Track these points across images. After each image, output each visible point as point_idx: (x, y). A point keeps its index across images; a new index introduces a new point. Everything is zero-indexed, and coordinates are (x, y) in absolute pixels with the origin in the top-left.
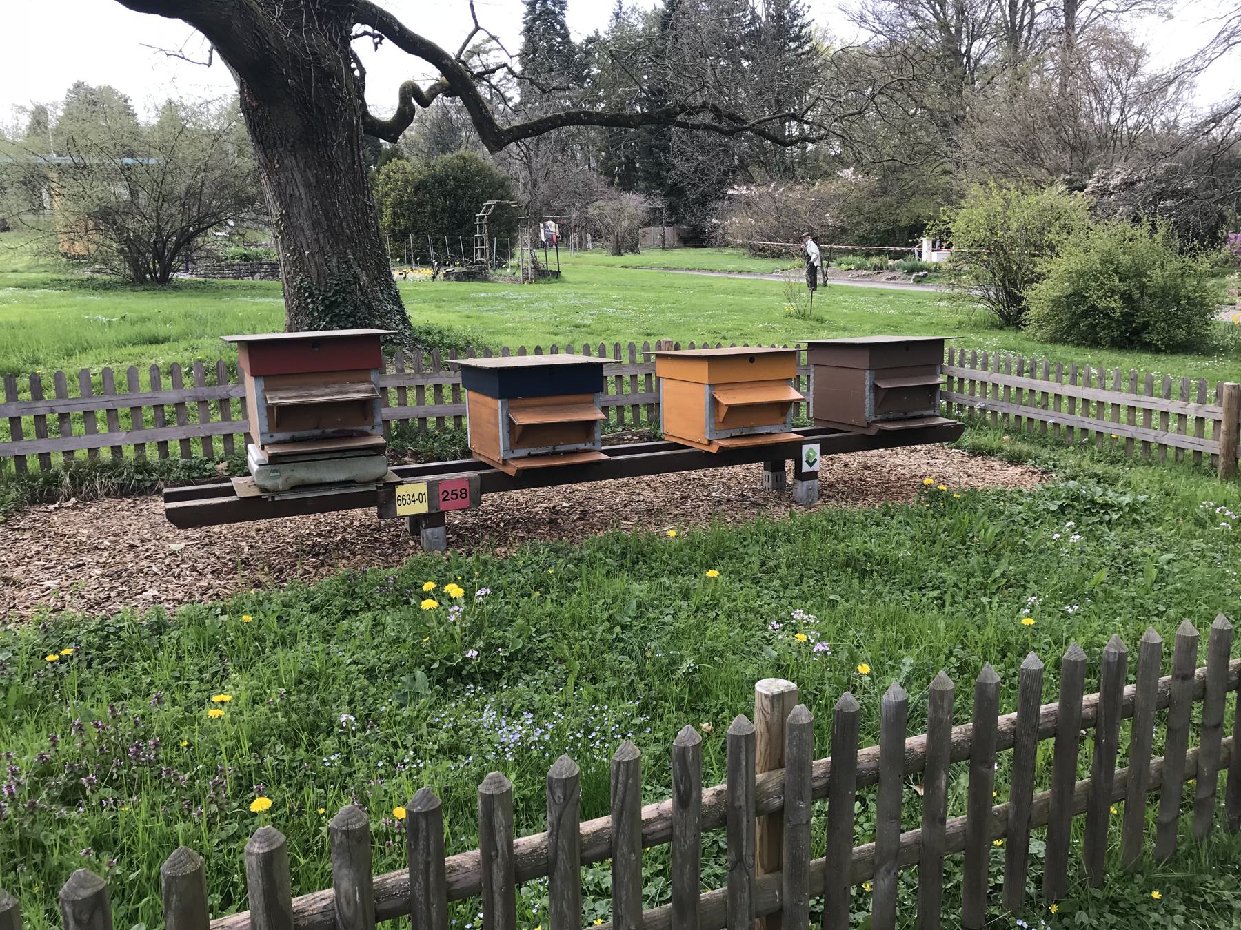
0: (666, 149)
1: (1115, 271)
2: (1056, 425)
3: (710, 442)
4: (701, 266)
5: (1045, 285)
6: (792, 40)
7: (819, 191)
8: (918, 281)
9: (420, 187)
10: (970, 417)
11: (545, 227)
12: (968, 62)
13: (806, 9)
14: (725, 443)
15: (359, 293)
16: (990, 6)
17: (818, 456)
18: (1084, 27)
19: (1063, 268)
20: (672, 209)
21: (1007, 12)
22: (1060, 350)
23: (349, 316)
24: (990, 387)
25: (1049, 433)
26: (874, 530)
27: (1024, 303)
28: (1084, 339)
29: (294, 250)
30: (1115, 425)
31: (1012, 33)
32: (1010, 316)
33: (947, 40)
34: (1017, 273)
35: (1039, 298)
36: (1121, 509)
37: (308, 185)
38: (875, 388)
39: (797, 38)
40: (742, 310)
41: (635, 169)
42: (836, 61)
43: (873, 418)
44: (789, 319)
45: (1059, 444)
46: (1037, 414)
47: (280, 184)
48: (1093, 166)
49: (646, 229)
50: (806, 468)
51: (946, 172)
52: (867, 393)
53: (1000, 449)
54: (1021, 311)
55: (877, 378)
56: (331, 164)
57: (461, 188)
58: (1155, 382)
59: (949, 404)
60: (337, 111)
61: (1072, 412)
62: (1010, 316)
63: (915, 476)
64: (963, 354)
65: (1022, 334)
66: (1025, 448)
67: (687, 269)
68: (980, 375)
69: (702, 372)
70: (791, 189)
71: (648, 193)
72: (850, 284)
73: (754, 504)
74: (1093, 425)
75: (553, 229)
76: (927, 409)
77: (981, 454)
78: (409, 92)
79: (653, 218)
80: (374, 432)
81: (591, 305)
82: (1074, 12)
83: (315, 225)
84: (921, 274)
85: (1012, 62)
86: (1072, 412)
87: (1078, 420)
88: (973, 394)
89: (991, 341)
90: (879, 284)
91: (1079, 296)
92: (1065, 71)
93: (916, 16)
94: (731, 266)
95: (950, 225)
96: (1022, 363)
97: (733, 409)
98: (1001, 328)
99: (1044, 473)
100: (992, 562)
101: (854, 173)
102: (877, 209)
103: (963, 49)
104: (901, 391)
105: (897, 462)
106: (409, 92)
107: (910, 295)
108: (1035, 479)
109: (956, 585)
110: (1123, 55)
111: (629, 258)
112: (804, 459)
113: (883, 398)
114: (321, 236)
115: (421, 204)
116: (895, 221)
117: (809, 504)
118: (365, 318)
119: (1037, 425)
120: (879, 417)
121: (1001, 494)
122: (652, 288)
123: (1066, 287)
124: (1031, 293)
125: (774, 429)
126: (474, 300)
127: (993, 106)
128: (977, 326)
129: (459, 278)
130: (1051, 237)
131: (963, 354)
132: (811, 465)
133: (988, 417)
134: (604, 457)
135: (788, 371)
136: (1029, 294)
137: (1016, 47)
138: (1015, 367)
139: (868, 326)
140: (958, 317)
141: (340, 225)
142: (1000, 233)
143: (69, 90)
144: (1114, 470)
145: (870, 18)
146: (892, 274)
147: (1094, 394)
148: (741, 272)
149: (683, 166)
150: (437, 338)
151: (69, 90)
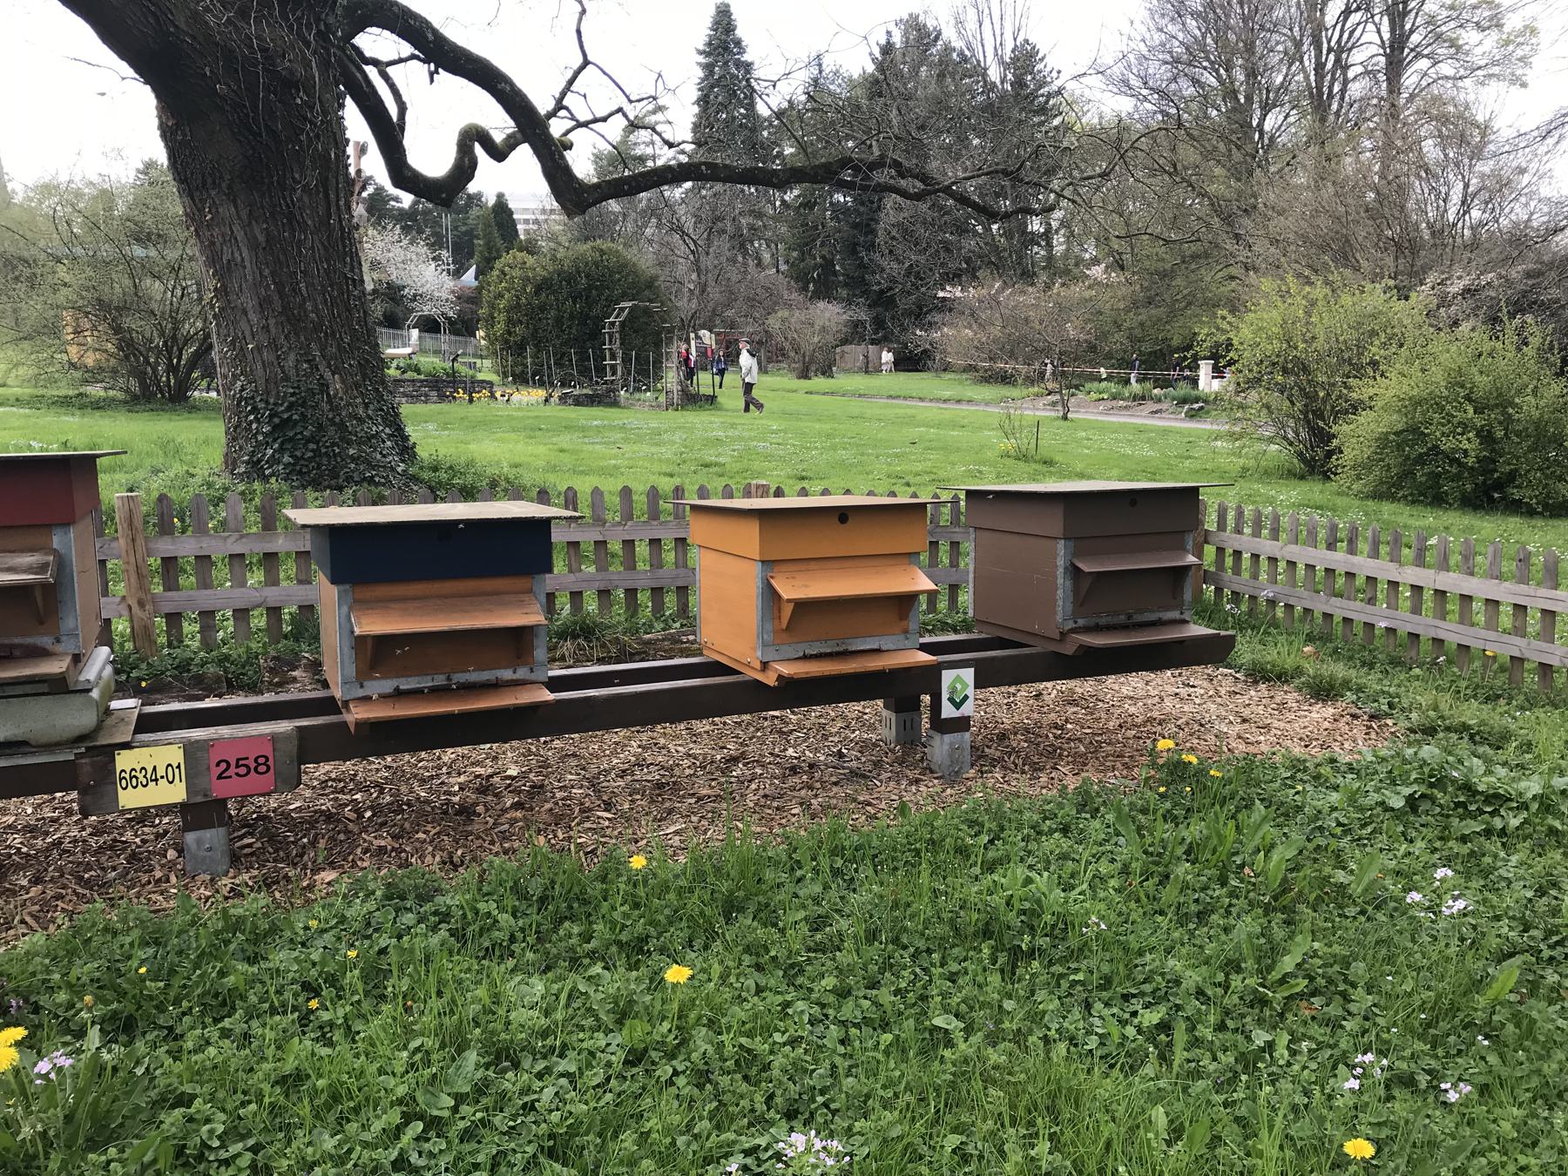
0: (871, 247)
1: (1468, 398)
2: (1391, 631)
3: (765, 666)
4: (907, 393)
5: (1364, 417)
6: (1037, 113)
7: (1058, 294)
8: (1192, 415)
9: (543, 286)
10: (1251, 612)
11: (698, 337)
12: (1262, 136)
13: (1054, 74)
14: (786, 669)
15: (326, 407)
16: (1289, 68)
17: (970, 691)
18: (1412, 96)
19: (1391, 393)
20: (879, 323)
21: (1312, 78)
22: (1387, 509)
23: (309, 441)
24: (1282, 566)
25: (1377, 643)
26: (1054, 843)
27: (1335, 442)
28: (1421, 494)
29: (233, 342)
30: (1491, 635)
31: (1319, 102)
32: (1316, 460)
33: (1234, 109)
34: (1324, 401)
35: (1355, 438)
36: (1524, 806)
37: (254, 246)
38: (1074, 572)
39: (1043, 110)
40: (945, 449)
41: (835, 273)
42: (1095, 136)
43: (1070, 625)
44: (1008, 461)
45: (1396, 662)
46: (1357, 610)
47: (212, 243)
48: (1426, 269)
49: (847, 348)
50: (948, 711)
51: (1233, 278)
52: (1060, 581)
53: (1299, 671)
54: (1329, 454)
55: (1076, 554)
56: (291, 217)
57: (596, 288)
58: (1534, 560)
59: (1219, 591)
60: (303, 137)
61: (1416, 610)
62: (1316, 460)
63: (1150, 720)
64: (1240, 513)
65: (1332, 486)
66: (1339, 670)
67: (890, 397)
68: (1267, 547)
69: (749, 537)
70: (1023, 292)
71: (849, 302)
72: (1100, 418)
73: (855, 774)
74: (1453, 632)
75: (707, 341)
76: (1168, 609)
77: (1267, 679)
78: (472, 137)
79: (854, 333)
80: (59, 648)
81: (740, 438)
82: (1399, 76)
83: (264, 304)
84: (1196, 406)
85: (1318, 139)
86: (1416, 610)
87: (1426, 625)
88: (1255, 576)
89: (1288, 495)
90: (1141, 418)
91: (1414, 432)
92: (1387, 151)
93: (1196, 82)
94: (947, 394)
95: (1231, 335)
96: (1334, 528)
97: (804, 607)
98: (1302, 478)
99: (1372, 717)
100: (1279, 933)
101: (1106, 272)
102: (1142, 324)
103: (1255, 124)
104: (1129, 576)
105: (1125, 691)
106: (472, 137)
107: (1179, 432)
108: (1358, 731)
109: (1200, 993)
110: (1466, 136)
111: (819, 382)
112: (945, 696)
113: (1088, 588)
114: (272, 321)
115: (542, 308)
116: (1164, 340)
117: (952, 777)
118: (334, 444)
119: (1358, 629)
120: (1081, 622)
121: (1297, 765)
122: (833, 418)
123: (1397, 421)
124: (1345, 427)
125: (886, 643)
126: (583, 429)
127: (1293, 195)
128: (1267, 474)
129: (578, 402)
130: (1375, 351)
131: (1240, 513)
132: (958, 706)
133: (1280, 612)
134: (548, 696)
135: (914, 539)
136: (1342, 429)
137: (1323, 120)
138: (1322, 534)
139: (1115, 472)
140: (1242, 461)
141: (302, 306)
142: (1301, 346)
143: (138, 171)
144: (1495, 717)
145: (1134, 82)
146: (1157, 407)
147: (1454, 582)
148: (959, 401)
149: (892, 267)
150: (444, 476)
151: (138, 171)
